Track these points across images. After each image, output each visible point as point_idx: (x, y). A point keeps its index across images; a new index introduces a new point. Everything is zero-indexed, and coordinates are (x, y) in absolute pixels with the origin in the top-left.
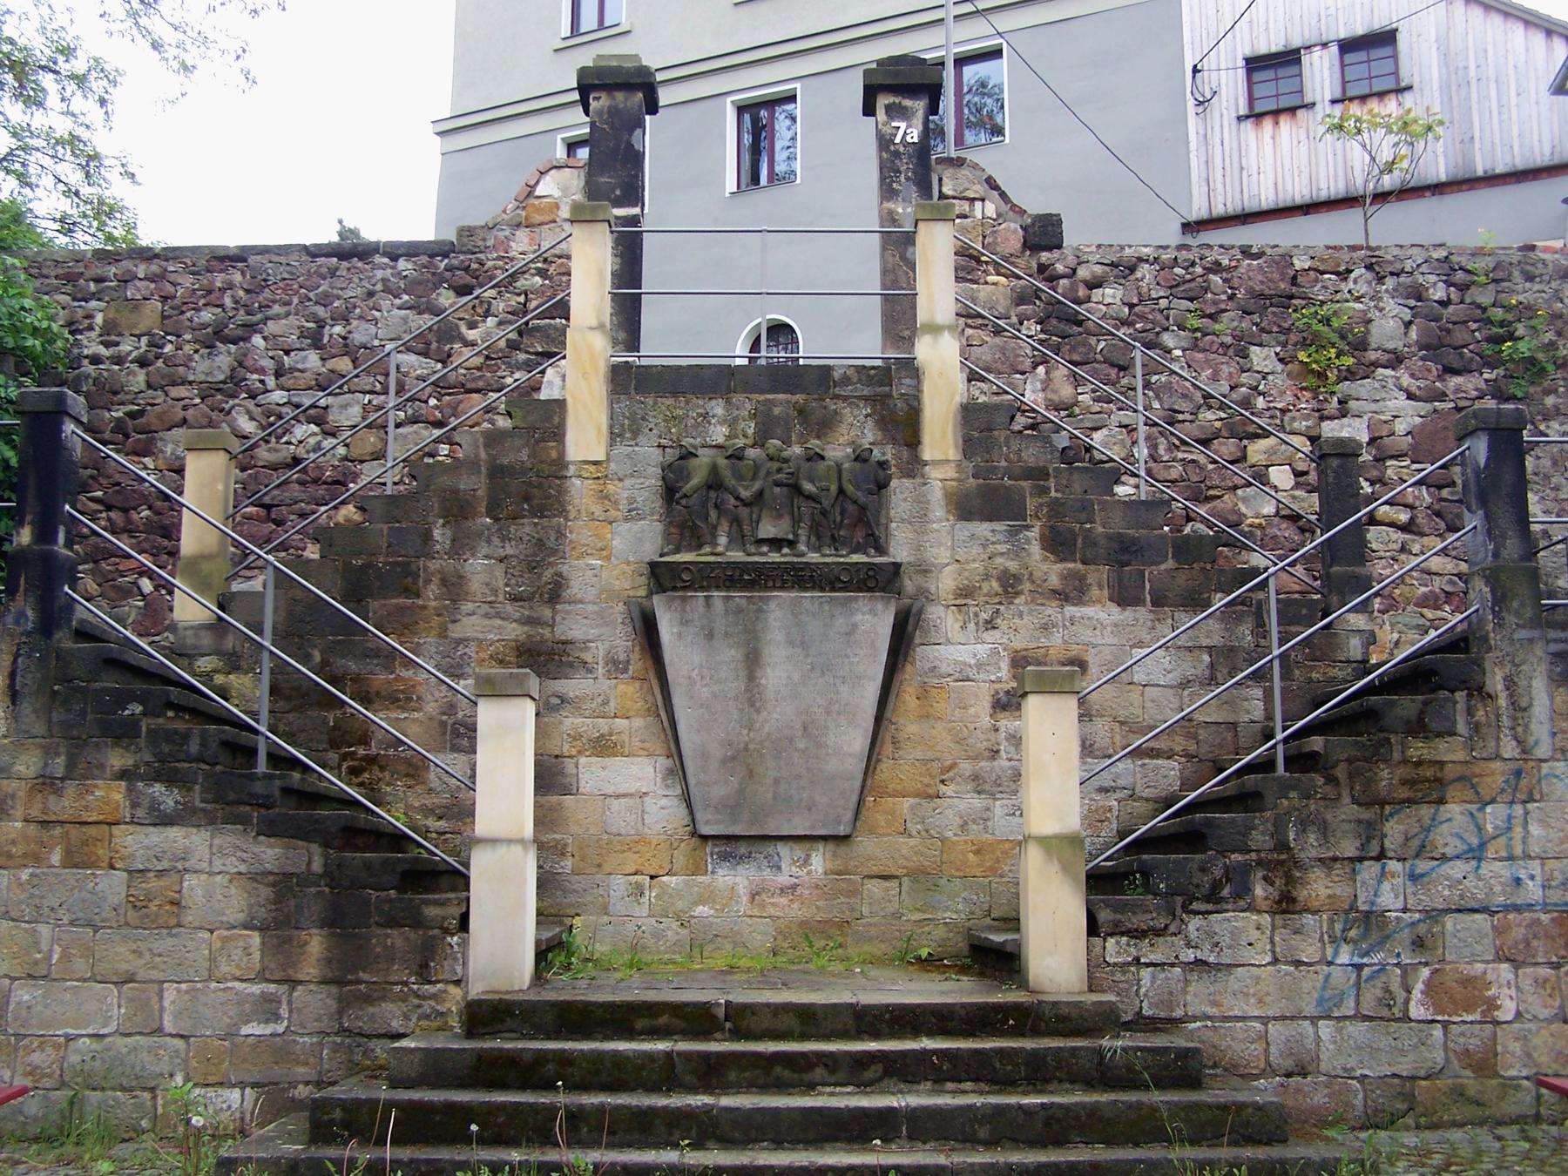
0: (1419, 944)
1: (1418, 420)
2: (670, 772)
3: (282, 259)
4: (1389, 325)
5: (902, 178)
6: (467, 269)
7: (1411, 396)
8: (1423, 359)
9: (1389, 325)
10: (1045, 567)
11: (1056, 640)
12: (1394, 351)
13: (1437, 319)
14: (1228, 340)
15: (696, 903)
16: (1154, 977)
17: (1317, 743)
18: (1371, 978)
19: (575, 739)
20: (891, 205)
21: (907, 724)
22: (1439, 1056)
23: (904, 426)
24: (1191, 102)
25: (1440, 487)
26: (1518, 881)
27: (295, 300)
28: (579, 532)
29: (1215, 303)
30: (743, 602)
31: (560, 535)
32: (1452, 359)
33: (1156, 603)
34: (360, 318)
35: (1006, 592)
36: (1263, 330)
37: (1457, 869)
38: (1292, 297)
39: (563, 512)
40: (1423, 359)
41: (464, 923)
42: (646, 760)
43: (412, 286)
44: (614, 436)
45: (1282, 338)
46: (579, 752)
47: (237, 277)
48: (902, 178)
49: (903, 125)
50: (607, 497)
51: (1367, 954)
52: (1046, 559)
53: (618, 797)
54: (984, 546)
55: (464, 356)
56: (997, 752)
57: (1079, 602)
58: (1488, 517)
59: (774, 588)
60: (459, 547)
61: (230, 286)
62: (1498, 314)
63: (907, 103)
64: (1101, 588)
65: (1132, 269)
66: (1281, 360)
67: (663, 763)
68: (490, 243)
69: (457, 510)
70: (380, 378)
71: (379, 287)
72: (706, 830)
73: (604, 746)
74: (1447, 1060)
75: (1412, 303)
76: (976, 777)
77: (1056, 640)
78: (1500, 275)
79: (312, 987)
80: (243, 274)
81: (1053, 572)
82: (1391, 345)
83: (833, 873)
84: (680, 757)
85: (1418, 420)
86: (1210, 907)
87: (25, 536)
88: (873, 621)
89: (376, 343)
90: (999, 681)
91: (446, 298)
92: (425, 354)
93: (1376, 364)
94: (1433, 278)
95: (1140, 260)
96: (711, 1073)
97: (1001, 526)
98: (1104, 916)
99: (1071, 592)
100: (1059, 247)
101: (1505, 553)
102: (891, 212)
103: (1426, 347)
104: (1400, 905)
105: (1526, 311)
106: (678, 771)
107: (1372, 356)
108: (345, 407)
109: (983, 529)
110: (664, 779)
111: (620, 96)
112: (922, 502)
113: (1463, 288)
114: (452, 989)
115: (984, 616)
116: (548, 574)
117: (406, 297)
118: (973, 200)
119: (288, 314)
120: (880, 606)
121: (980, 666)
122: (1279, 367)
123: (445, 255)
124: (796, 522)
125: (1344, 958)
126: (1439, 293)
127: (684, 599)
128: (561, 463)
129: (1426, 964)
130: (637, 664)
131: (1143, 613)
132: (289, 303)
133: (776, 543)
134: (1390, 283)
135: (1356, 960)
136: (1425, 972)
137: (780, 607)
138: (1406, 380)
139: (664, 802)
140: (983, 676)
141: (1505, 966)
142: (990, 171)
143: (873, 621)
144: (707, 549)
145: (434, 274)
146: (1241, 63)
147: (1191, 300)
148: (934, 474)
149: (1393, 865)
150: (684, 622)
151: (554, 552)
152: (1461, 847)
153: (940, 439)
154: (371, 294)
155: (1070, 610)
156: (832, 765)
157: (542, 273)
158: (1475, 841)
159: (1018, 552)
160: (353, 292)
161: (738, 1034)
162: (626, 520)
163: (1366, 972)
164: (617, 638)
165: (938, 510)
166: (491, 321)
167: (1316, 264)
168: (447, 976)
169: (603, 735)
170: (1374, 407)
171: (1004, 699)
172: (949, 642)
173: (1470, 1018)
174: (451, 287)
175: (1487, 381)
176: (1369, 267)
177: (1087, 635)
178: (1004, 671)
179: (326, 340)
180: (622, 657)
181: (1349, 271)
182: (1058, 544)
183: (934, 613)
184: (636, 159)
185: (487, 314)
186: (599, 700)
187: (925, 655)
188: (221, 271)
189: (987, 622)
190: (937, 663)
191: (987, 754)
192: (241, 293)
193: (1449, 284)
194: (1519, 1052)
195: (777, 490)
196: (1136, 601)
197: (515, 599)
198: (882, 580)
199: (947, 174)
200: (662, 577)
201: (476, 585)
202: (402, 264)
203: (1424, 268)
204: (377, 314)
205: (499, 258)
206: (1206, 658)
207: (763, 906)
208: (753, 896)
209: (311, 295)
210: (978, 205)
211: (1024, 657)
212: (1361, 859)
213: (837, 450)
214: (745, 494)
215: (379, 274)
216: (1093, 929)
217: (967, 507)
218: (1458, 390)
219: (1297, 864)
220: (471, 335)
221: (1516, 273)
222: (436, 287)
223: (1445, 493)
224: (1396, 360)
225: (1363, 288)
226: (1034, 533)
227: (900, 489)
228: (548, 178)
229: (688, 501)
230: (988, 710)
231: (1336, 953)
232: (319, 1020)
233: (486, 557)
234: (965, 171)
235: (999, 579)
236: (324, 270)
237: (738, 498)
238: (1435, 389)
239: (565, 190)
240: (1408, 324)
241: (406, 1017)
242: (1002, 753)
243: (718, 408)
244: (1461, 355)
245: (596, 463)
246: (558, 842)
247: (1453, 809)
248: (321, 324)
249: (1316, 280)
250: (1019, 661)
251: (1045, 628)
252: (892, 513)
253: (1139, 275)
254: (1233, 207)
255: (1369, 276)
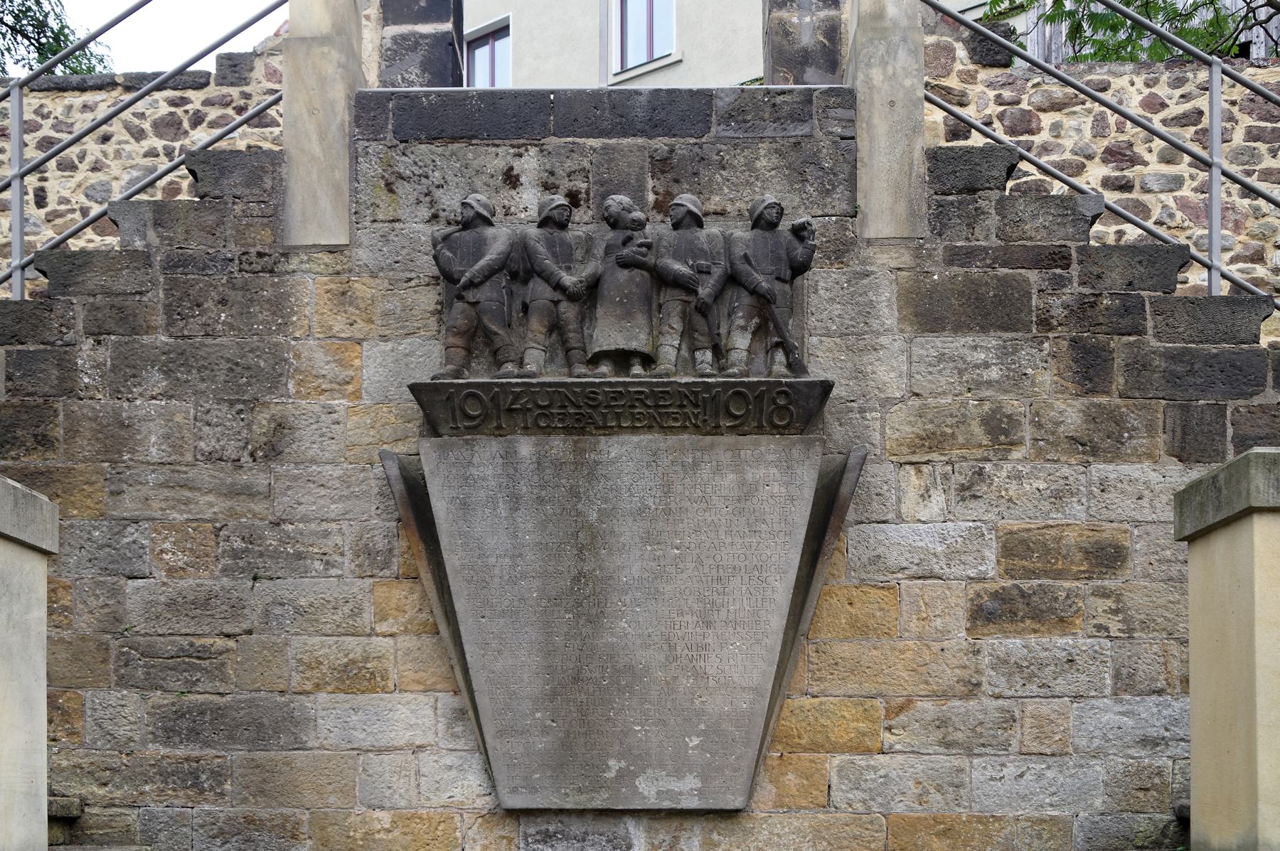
2: (460, 714)
10: (1060, 405)
11: (1077, 511)
19: (310, 667)
20: (783, 14)
35: (995, 440)
42: (421, 697)
46: (318, 687)
53: (380, 751)
56: (978, 685)
57: (1116, 456)
60: (123, 375)
67: (447, 701)
69: (118, 319)
73: (357, 678)
76: (942, 723)
81: (1070, 413)
84: (471, 692)
90: (981, 579)
102: (782, 23)
106: (469, 713)
110: (449, 726)
116: (262, 419)
130: (405, 547)
137: (625, 455)
139: (449, 760)
143: (778, 481)
144: (509, 367)
148: (884, 260)
155: (1099, 469)
156: (716, 704)
164: (376, 521)
165: (888, 313)
169: (353, 662)
172: (900, 519)
177: (1124, 506)
180: (381, 544)
182: (1089, 369)
183: (879, 474)
186: (346, 609)
187: (856, 541)
189: (963, 488)
190: (881, 550)
191: (960, 688)
195: (623, 275)
198: (795, 408)
200: (441, 408)
211: (1023, 542)
214: (568, 279)
217: (927, 313)
227: (823, 281)
229: (483, 290)
230: (964, 623)
237: (559, 287)
242: (985, 687)
245: (332, 250)
246: (286, 819)
252: (812, 322)
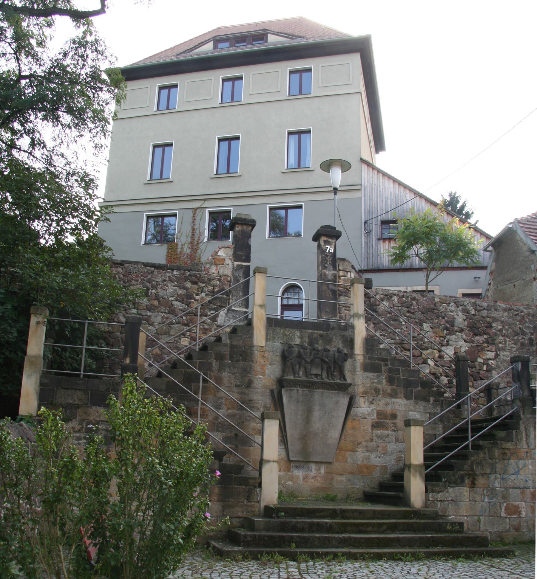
0: (504, 497)
1: (467, 348)
3: (136, 266)
4: (460, 319)
5: (328, 263)
6: (196, 276)
7: (465, 341)
8: (469, 331)
9: (460, 319)
12: (461, 328)
13: (472, 320)
14: (417, 321)
15: (288, 481)
16: (441, 504)
17: (481, 442)
18: (493, 505)
21: (349, 430)
22: (508, 526)
23: (350, 343)
24: (363, 232)
25: (472, 368)
26: (526, 481)
27: (140, 280)
28: (257, 367)
29: (414, 309)
30: (308, 392)
31: (251, 367)
32: (476, 331)
33: (416, 399)
34: (161, 288)
36: (427, 319)
37: (513, 477)
38: (434, 309)
39: (252, 361)
40: (469, 331)
41: (260, 485)
43: (178, 279)
44: (267, 339)
45: (432, 321)
47: (121, 270)
48: (328, 263)
49: (329, 247)
50: (265, 357)
51: (491, 499)
52: (387, 385)
54: (371, 380)
55: (195, 305)
58: (521, 384)
59: (316, 389)
60: (221, 368)
61: (118, 273)
62: (488, 320)
63: (330, 240)
64: (401, 393)
65: (391, 297)
66: (431, 328)
68: (203, 269)
70: (168, 308)
71: (167, 279)
72: (292, 459)
74: (510, 528)
75: (466, 314)
76: (367, 447)
77: (389, 408)
78: (488, 308)
79: (215, 503)
80: (122, 269)
82: (460, 326)
83: (327, 473)
85: (467, 348)
86: (455, 485)
87: (128, 361)
88: (344, 401)
89: (166, 297)
90: (373, 419)
91: (189, 285)
92: (182, 302)
93: (457, 331)
94: (471, 308)
95: (393, 294)
96: (344, 528)
97: (375, 374)
98: (429, 487)
99: (393, 395)
100: (371, 288)
101: (524, 394)
103: (470, 327)
104: (499, 486)
105: (495, 320)
107: (456, 329)
108: (156, 316)
109: (370, 375)
111: (245, 227)
112: (354, 366)
113: (479, 311)
114: (256, 504)
115: (370, 400)
117: (176, 283)
118: (347, 272)
119: (137, 284)
120: (345, 396)
121: (369, 414)
122: (431, 330)
123: (189, 271)
124: (322, 369)
125: (486, 500)
126: (473, 312)
127: (291, 390)
128: (252, 346)
129: (505, 502)
131: (412, 402)
132: (137, 281)
133: (316, 375)
134: (460, 308)
135: (489, 501)
136: (505, 504)
137: (318, 394)
138: (464, 336)
140: (369, 417)
141: (523, 503)
142: (353, 264)
145: (185, 277)
146: (379, 223)
147: (407, 308)
149: (498, 476)
150: (290, 397)
151: (249, 373)
152: (514, 471)
153: (359, 348)
154: (165, 281)
155: (393, 400)
157: (219, 280)
158: (517, 470)
159: (380, 382)
160: (159, 279)
161: (343, 518)
162: (270, 365)
163: (491, 504)
166: (203, 294)
167: (441, 301)
168: (255, 500)
170: (456, 343)
171: (375, 425)
172: (360, 407)
173: (515, 516)
174: (190, 281)
175: (485, 338)
176: (455, 303)
177: (397, 407)
178: (375, 417)
179: (150, 294)
180: (268, 406)
181: (450, 303)
182: (391, 381)
184: (249, 247)
185: (202, 291)
187: (354, 410)
188: (115, 268)
192: (122, 276)
193: (475, 310)
194: (525, 525)
196: (411, 399)
197: (237, 386)
198: (343, 388)
199: (341, 263)
200: (281, 383)
201: (225, 381)
202: (175, 272)
203: (469, 305)
204: (167, 287)
205: (206, 274)
206: (428, 415)
207: (307, 482)
208: (304, 479)
209: (145, 279)
210: (349, 273)
212: (491, 474)
213: (333, 349)
215: (168, 275)
216: (426, 491)
218: (478, 340)
219: (475, 475)
220: (197, 298)
221: (493, 308)
222: (186, 281)
223: (474, 369)
224: (462, 330)
225: (453, 309)
226: (384, 377)
228: (222, 250)
231: (484, 499)
232: (217, 512)
233: (228, 373)
234: (346, 263)
235: (374, 390)
236: (149, 271)
238: (471, 339)
239: (227, 254)
240: (465, 320)
241: (243, 512)
243: (298, 333)
244: (478, 330)
245: (262, 347)
247: (512, 461)
248: (148, 289)
249: (441, 305)
250: (380, 414)
251: (386, 404)
253: (393, 299)
254: (375, 267)
255: (455, 305)
